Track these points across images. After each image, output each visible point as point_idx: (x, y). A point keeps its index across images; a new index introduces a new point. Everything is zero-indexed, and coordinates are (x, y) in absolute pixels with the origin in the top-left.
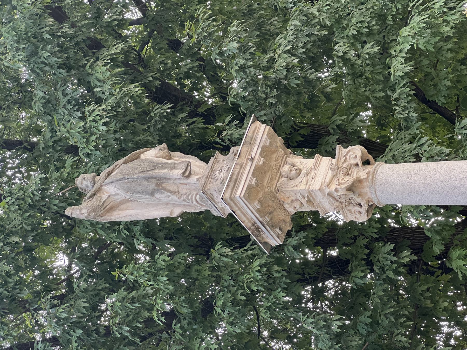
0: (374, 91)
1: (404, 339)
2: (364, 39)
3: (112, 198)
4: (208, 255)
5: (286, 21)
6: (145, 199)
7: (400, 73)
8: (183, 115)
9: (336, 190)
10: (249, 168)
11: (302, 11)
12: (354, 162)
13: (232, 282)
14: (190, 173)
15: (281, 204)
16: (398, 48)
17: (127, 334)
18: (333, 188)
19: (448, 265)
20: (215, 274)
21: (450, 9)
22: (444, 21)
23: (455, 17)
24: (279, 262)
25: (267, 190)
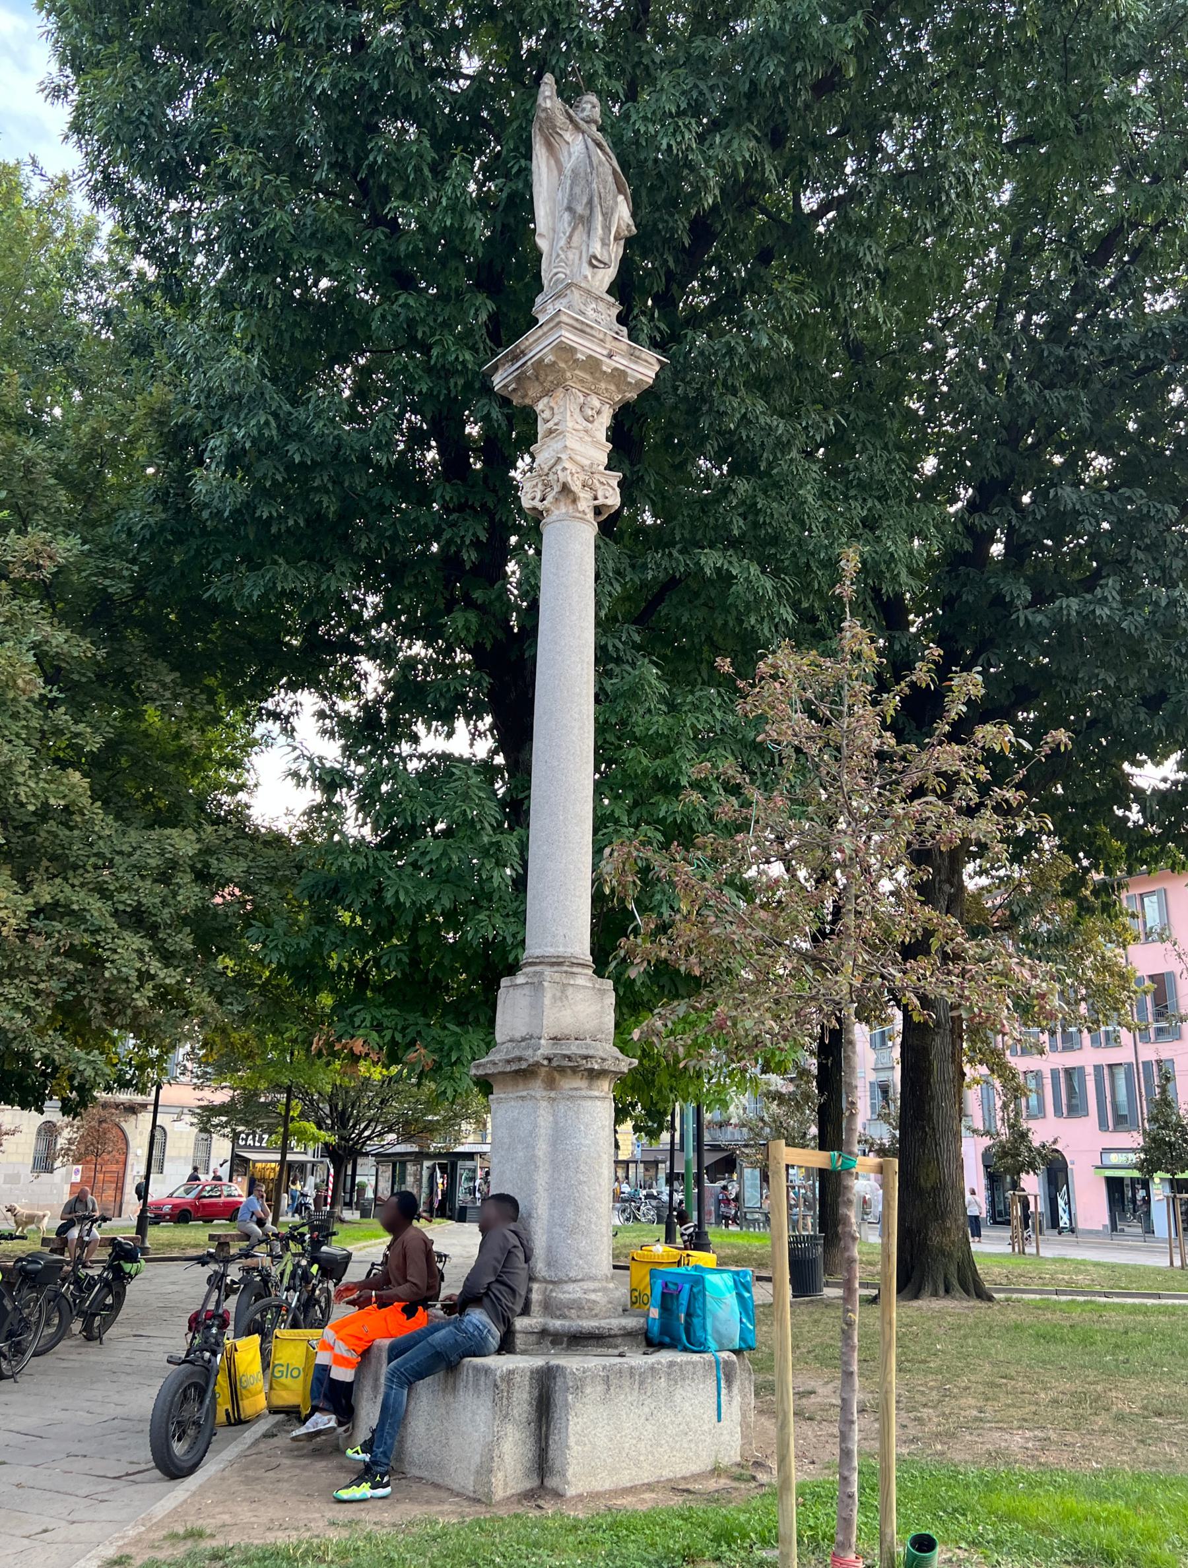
0: (682, 526)
1: (363, 545)
2: (750, 517)
3: (565, 147)
4: (479, 286)
5: (781, 416)
6: (562, 198)
7: (703, 560)
8: (671, 264)
9: (564, 469)
10: (599, 352)
11: (794, 437)
12: (600, 494)
13: (440, 319)
14: (594, 267)
15: (548, 393)
16: (734, 559)
17: (371, 158)
18: (567, 465)
19: (457, 607)
20: (453, 295)
21: (776, 626)
22: (763, 618)
23: (766, 631)
24: (468, 386)
25: (568, 374)
